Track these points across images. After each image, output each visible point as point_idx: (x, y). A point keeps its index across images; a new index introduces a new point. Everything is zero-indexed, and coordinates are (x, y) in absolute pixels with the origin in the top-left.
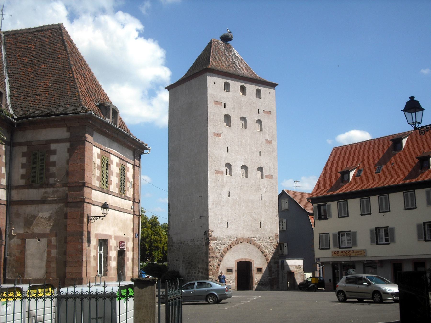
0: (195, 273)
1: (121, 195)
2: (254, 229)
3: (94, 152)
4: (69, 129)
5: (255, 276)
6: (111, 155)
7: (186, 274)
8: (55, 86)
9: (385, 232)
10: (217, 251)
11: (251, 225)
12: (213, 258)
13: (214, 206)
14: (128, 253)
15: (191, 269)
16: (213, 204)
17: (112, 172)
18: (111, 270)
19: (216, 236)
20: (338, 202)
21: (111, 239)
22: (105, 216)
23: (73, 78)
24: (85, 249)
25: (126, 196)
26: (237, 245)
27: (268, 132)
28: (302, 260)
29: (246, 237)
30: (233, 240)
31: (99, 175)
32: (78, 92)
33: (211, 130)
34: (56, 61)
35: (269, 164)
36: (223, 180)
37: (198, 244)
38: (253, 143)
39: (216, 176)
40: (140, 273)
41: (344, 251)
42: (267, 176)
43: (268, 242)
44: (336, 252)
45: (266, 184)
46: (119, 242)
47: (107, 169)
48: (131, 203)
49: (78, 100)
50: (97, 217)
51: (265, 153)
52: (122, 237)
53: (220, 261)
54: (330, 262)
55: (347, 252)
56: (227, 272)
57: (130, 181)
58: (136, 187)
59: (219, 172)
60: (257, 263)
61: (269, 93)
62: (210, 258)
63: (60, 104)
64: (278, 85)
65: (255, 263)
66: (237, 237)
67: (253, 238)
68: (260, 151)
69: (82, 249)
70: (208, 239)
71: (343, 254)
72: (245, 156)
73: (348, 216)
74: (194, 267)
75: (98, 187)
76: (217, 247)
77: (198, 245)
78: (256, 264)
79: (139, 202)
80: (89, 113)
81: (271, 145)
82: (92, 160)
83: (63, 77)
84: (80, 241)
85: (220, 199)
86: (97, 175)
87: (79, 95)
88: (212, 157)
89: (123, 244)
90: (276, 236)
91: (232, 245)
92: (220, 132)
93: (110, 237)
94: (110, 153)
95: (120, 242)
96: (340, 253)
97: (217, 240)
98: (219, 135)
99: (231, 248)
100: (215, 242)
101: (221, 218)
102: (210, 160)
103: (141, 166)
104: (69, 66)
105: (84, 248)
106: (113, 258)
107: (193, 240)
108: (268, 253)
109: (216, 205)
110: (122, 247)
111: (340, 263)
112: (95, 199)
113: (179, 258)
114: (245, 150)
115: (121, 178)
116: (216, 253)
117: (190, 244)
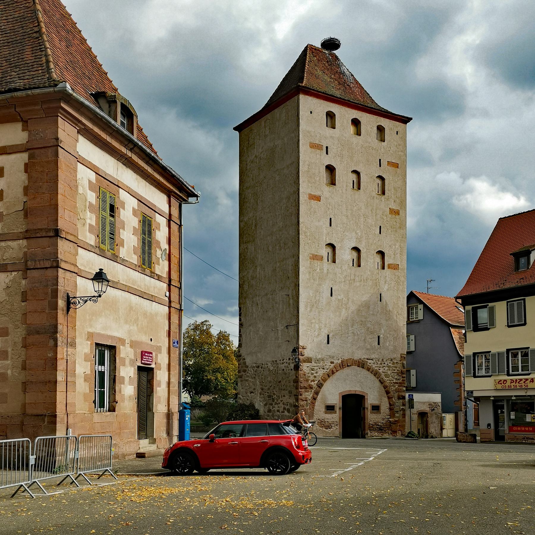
0: (278, 411)
1: (144, 270)
2: (369, 347)
3: (79, 176)
4: (25, 124)
5: (369, 417)
6: (120, 190)
7: (265, 412)
8: (5, 50)
9: (522, 364)
10: (312, 378)
11: (364, 340)
12: (305, 388)
13: (309, 309)
14: (158, 372)
15: (272, 404)
16: (306, 306)
17: (123, 223)
18: (123, 401)
19: (310, 356)
20: (507, 302)
21: (124, 345)
22: (100, 296)
23: (39, 34)
24: (62, 359)
25: (154, 273)
26: (342, 370)
27: (393, 197)
28: (440, 394)
29: (355, 358)
30: (335, 362)
31: (94, 223)
32: (46, 56)
33: (305, 189)
34: (11, 8)
35: (394, 246)
36: (323, 269)
37: (284, 368)
38: (370, 212)
39: (312, 263)
40: (181, 408)
41: (516, 380)
42: (390, 266)
43: (389, 367)
44: (502, 382)
45: (388, 277)
46: (139, 352)
47: (113, 216)
48: (165, 286)
49: (45, 70)
50: (86, 298)
51: (387, 229)
52: (148, 344)
53: (317, 393)
54: (490, 397)
55: (522, 382)
56: (327, 410)
57: (163, 249)
58: (174, 260)
59: (316, 257)
60: (372, 397)
61: (397, 134)
62: (301, 388)
63: (11, 80)
64: (411, 119)
65: (369, 398)
66: (343, 358)
67: (367, 359)
68: (380, 227)
69: (55, 359)
70: (299, 359)
71: (514, 384)
72: (356, 233)
73: (525, 324)
74: (278, 402)
75: (91, 245)
76: (313, 372)
77: (283, 370)
78: (371, 399)
79: (179, 286)
80: (61, 85)
81: (397, 217)
82: (77, 190)
83: (22, 34)
84: (52, 343)
85: (317, 298)
86: (88, 221)
87: (48, 62)
88: (305, 233)
89: (148, 356)
90: (401, 357)
91: (334, 370)
92: (317, 193)
93: (122, 341)
94: (119, 187)
95: (142, 352)
96: (508, 383)
97: (313, 362)
98: (318, 198)
99: (334, 374)
100: (308, 364)
101: (318, 327)
102: (303, 237)
103: (182, 224)
104: (34, 14)
105: (59, 356)
106: (127, 380)
107: (276, 361)
108: (389, 383)
109: (311, 308)
110: (147, 361)
111: (508, 399)
112: (84, 266)
113: (254, 389)
114: (357, 224)
115: (144, 239)
116: (310, 381)
117: (272, 368)
